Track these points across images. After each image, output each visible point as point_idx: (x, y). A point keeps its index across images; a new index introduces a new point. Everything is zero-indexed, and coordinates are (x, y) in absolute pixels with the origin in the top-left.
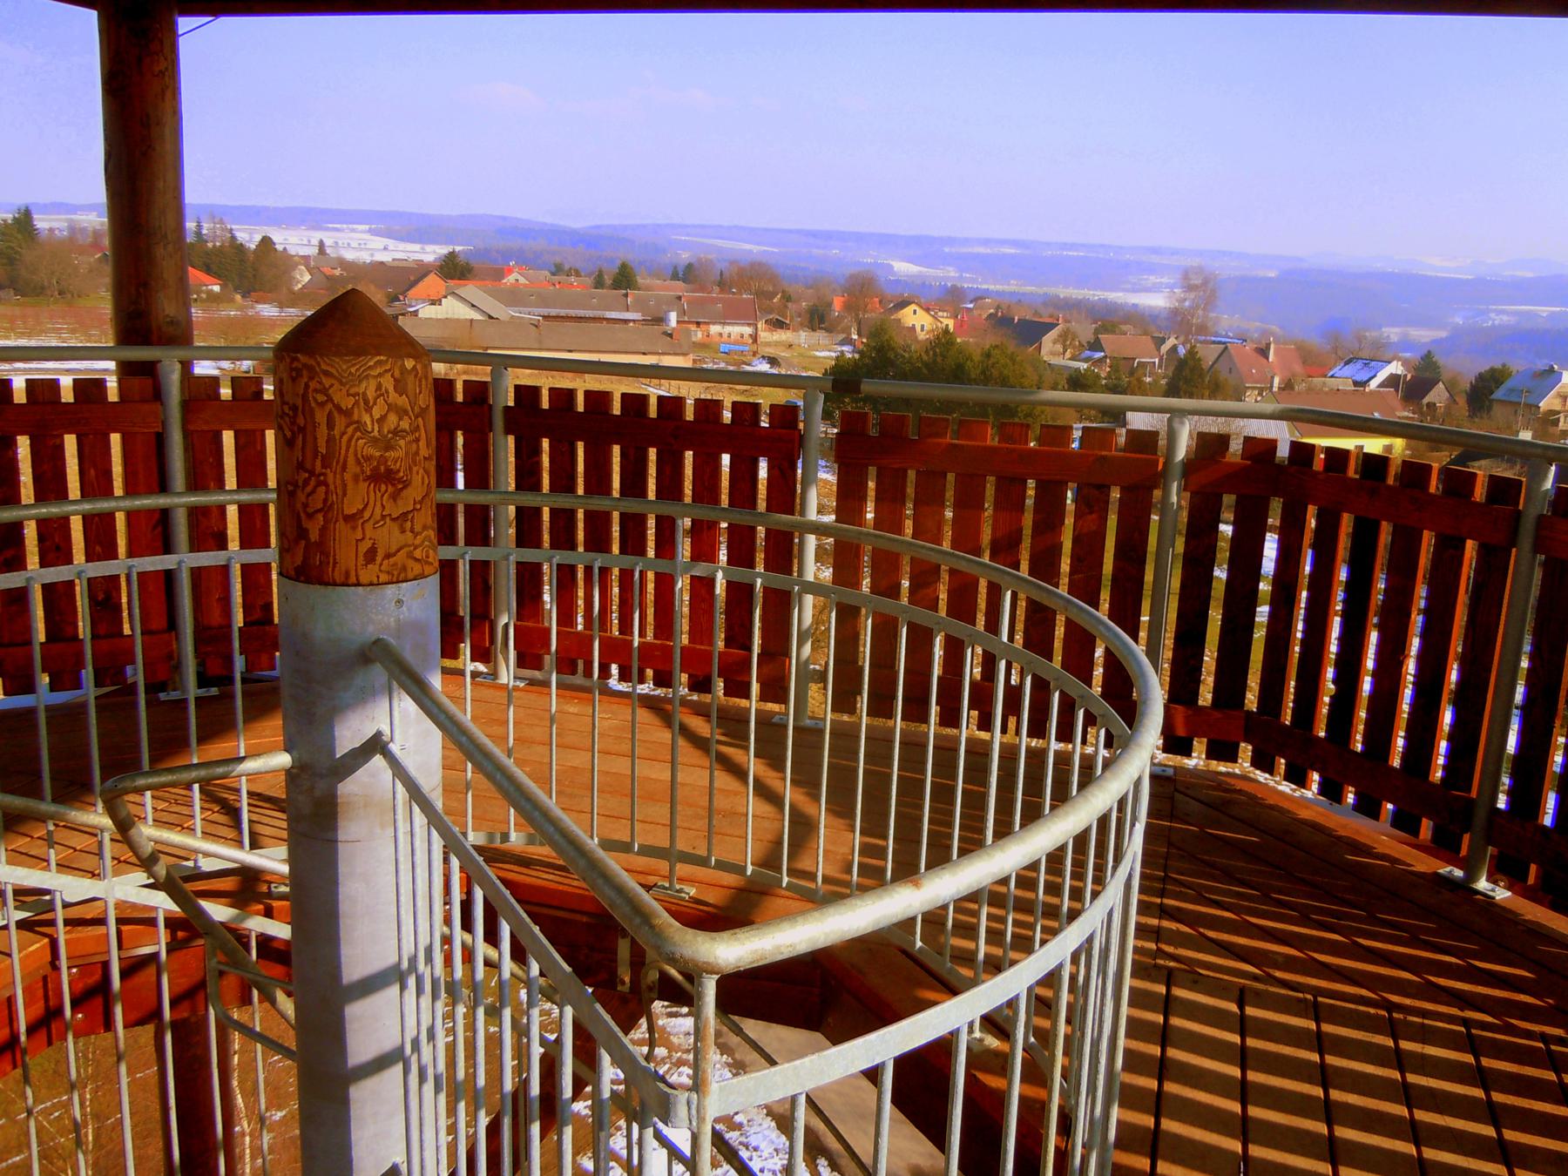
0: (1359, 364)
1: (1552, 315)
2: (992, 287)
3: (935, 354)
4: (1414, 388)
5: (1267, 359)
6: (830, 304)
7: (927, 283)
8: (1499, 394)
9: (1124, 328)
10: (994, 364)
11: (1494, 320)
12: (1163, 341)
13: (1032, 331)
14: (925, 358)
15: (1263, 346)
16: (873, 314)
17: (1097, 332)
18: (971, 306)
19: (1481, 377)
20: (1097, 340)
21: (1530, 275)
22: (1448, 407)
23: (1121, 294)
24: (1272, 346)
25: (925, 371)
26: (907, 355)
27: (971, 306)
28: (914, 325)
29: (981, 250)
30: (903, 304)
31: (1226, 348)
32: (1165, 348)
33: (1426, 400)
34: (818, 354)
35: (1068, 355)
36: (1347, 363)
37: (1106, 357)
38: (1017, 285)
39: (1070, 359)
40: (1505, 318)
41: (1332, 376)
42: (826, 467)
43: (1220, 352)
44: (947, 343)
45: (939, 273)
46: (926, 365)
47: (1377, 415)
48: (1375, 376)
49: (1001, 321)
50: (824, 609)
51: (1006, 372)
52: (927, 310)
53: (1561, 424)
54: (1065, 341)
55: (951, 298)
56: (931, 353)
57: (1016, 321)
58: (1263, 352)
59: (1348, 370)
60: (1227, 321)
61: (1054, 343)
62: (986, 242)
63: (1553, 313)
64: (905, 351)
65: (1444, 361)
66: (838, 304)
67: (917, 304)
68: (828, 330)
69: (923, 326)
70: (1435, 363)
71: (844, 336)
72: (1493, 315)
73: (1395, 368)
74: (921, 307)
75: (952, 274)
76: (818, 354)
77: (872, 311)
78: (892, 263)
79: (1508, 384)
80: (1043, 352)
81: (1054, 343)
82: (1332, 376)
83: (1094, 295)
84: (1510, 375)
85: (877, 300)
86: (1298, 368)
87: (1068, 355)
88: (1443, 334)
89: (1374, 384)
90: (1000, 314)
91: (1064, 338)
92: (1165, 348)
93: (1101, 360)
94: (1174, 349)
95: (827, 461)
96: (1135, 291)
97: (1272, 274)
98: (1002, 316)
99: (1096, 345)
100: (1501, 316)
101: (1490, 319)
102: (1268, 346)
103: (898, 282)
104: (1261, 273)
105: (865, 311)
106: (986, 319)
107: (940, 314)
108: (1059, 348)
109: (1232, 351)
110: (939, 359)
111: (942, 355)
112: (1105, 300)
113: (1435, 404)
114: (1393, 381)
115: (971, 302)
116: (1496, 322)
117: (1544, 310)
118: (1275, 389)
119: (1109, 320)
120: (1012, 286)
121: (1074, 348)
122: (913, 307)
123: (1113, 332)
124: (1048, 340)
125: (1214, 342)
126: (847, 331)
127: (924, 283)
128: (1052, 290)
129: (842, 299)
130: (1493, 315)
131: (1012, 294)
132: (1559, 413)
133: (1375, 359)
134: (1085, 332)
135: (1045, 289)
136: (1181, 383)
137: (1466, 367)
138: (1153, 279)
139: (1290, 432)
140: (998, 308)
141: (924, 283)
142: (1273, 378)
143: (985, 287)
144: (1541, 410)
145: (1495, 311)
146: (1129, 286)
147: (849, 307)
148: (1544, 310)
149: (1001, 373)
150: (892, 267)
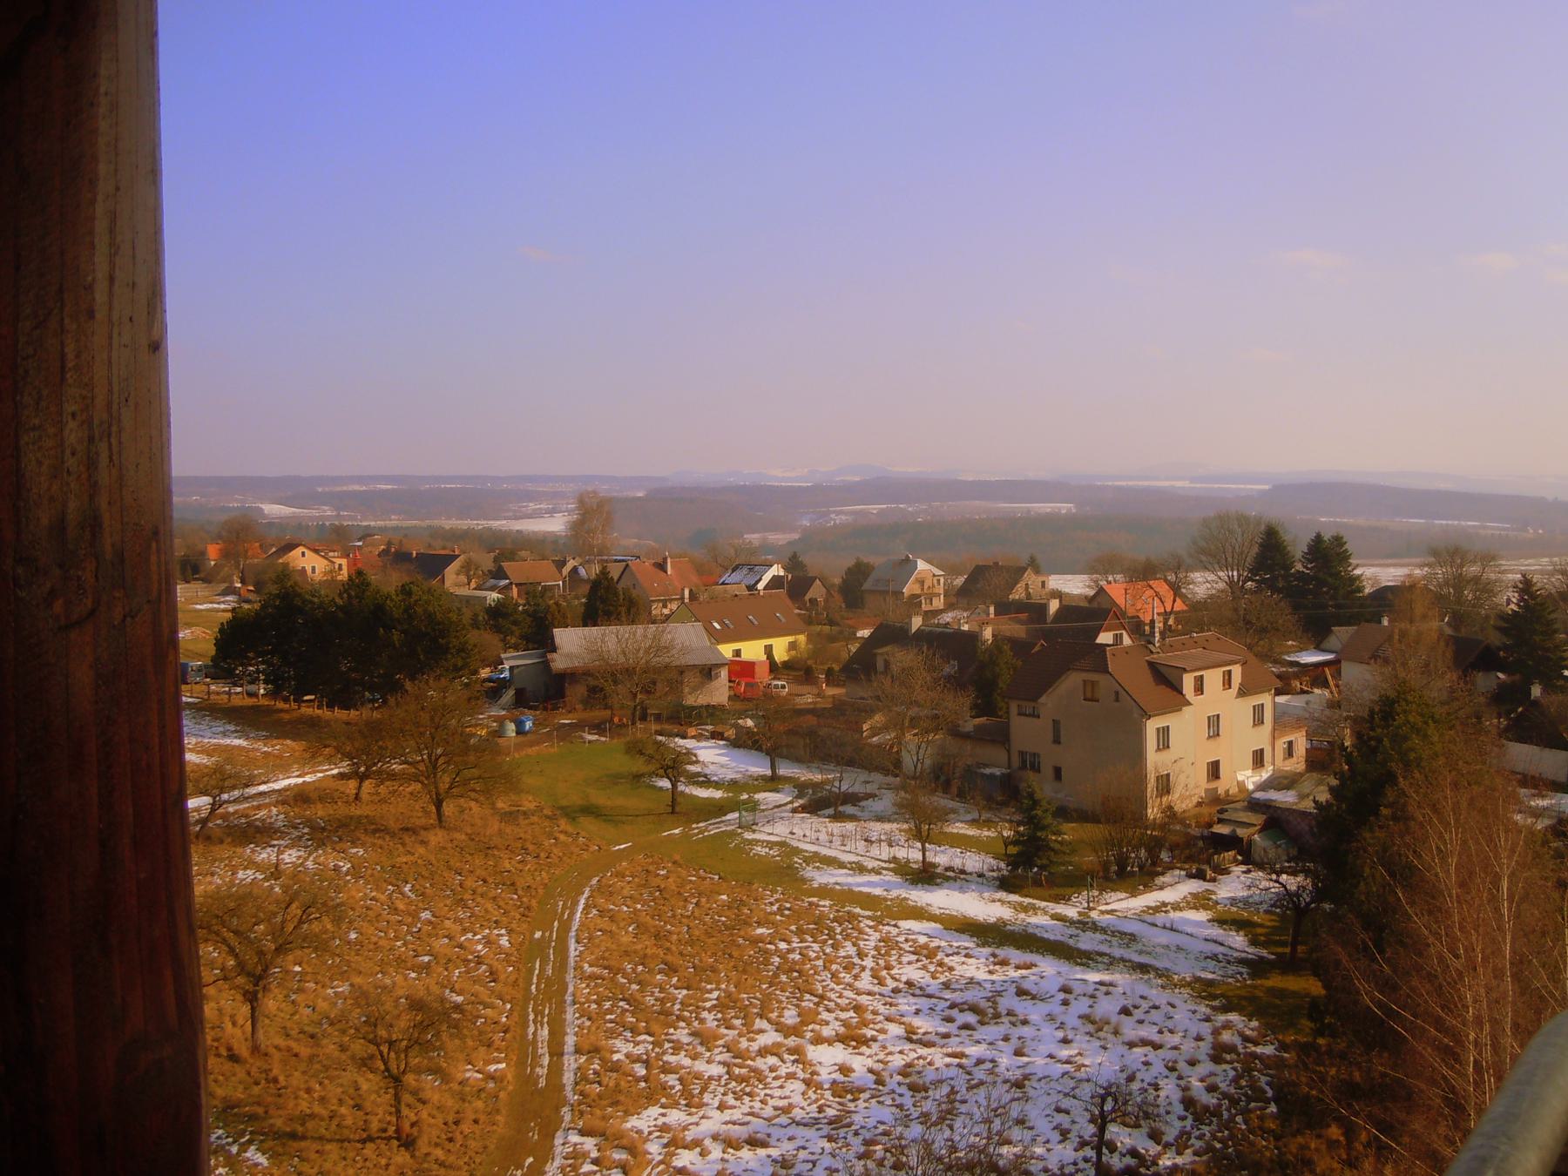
0: (745, 570)
1: (881, 511)
2: (373, 523)
3: (350, 596)
4: (796, 585)
5: (666, 572)
6: (203, 553)
7: (304, 523)
8: (867, 586)
9: (523, 554)
10: (416, 601)
11: (835, 520)
12: (564, 563)
13: (434, 564)
14: (340, 602)
15: (660, 561)
16: (257, 559)
17: (496, 560)
18: (360, 543)
19: (849, 571)
20: (500, 569)
21: (857, 479)
22: (826, 601)
23: (505, 522)
24: (669, 560)
25: (341, 615)
26: (316, 600)
27: (360, 543)
28: (304, 568)
29: (357, 488)
30: (290, 547)
31: (627, 565)
32: (566, 570)
33: (807, 598)
34: (199, 607)
35: (473, 585)
36: (733, 571)
37: (511, 583)
38: (398, 520)
39: (475, 589)
40: (843, 517)
41: (723, 584)
42: (236, 731)
43: (622, 569)
44: (363, 584)
45: (315, 513)
46: (340, 608)
47: (865, 633)
48: (760, 579)
49: (399, 557)
50: (1093, 1022)
51: (431, 609)
52: (316, 551)
53: (923, 606)
54: (469, 570)
55: (333, 539)
56: (345, 595)
57: (414, 555)
58: (661, 567)
59: (736, 577)
60: (624, 540)
61: (458, 574)
62: (360, 480)
63: (882, 509)
64: (313, 596)
65: (813, 562)
66: (213, 553)
67: (304, 546)
68: (207, 580)
69: (314, 568)
70: (801, 562)
71: (226, 585)
72: (833, 516)
73: (776, 570)
74: (309, 548)
75: (329, 513)
76: (199, 607)
77: (254, 557)
78: (263, 506)
79: (874, 575)
80: (448, 583)
81: (458, 574)
82: (723, 584)
83: (478, 524)
84: (874, 568)
85: (257, 544)
86: (694, 579)
87: (473, 585)
88: (796, 536)
89: (761, 586)
90: (393, 550)
91: (467, 568)
92: (566, 570)
93: (508, 587)
94: (575, 570)
95: (236, 725)
96: (516, 518)
97: (640, 494)
98: (396, 551)
99: (499, 573)
100: (840, 516)
101: (831, 519)
102: (665, 559)
103: (271, 524)
104: (631, 494)
105: (246, 557)
106: (379, 555)
107: (331, 554)
108: (463, 578)
109: (634, 568)
110: (355, 602)
111: (357, 597)
112: (490, 529)
113: (816, 599)
114: (776, 582)
115: (359, 540)
116: (838, 522)
117: (874, 508)
118: (686, 601)
119: (505, 550)
120: (394, 521)
121: (478, 577)
122: (301, 549)
123: (513, 560)
124: (451, 574)
125: (616, 561)
126: (228, 579)
127: (300, 524)
128: (436, 523)
129: (218, 547)
130: (833, 516)
131: (396, 529)
132: (919, 596)
133: (755, 566)
134: (487, 561)
135: (428, 522)
136: (598, 603)
137: (834, 567)
138: (532, 506)
139: (710, 640)
140: (389, 544)
141: (300, 524)
142: (683, 590)
143: (365, 524)
144: (906, 595)
145: (834, 512)
146: (511, 514)
147: (226, 554)
148: (874, 508)
149: (425, 611)
150: (262, 510)
